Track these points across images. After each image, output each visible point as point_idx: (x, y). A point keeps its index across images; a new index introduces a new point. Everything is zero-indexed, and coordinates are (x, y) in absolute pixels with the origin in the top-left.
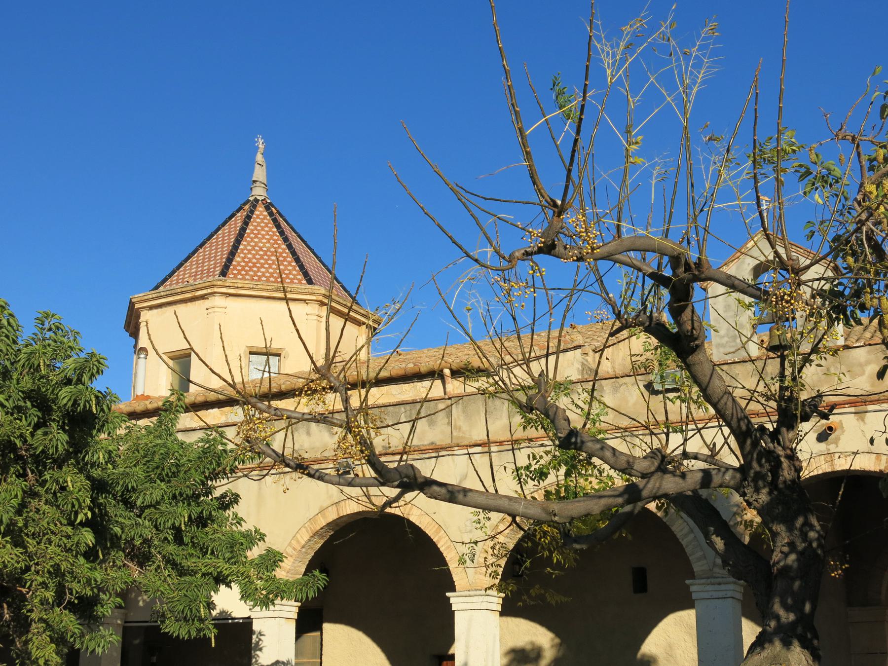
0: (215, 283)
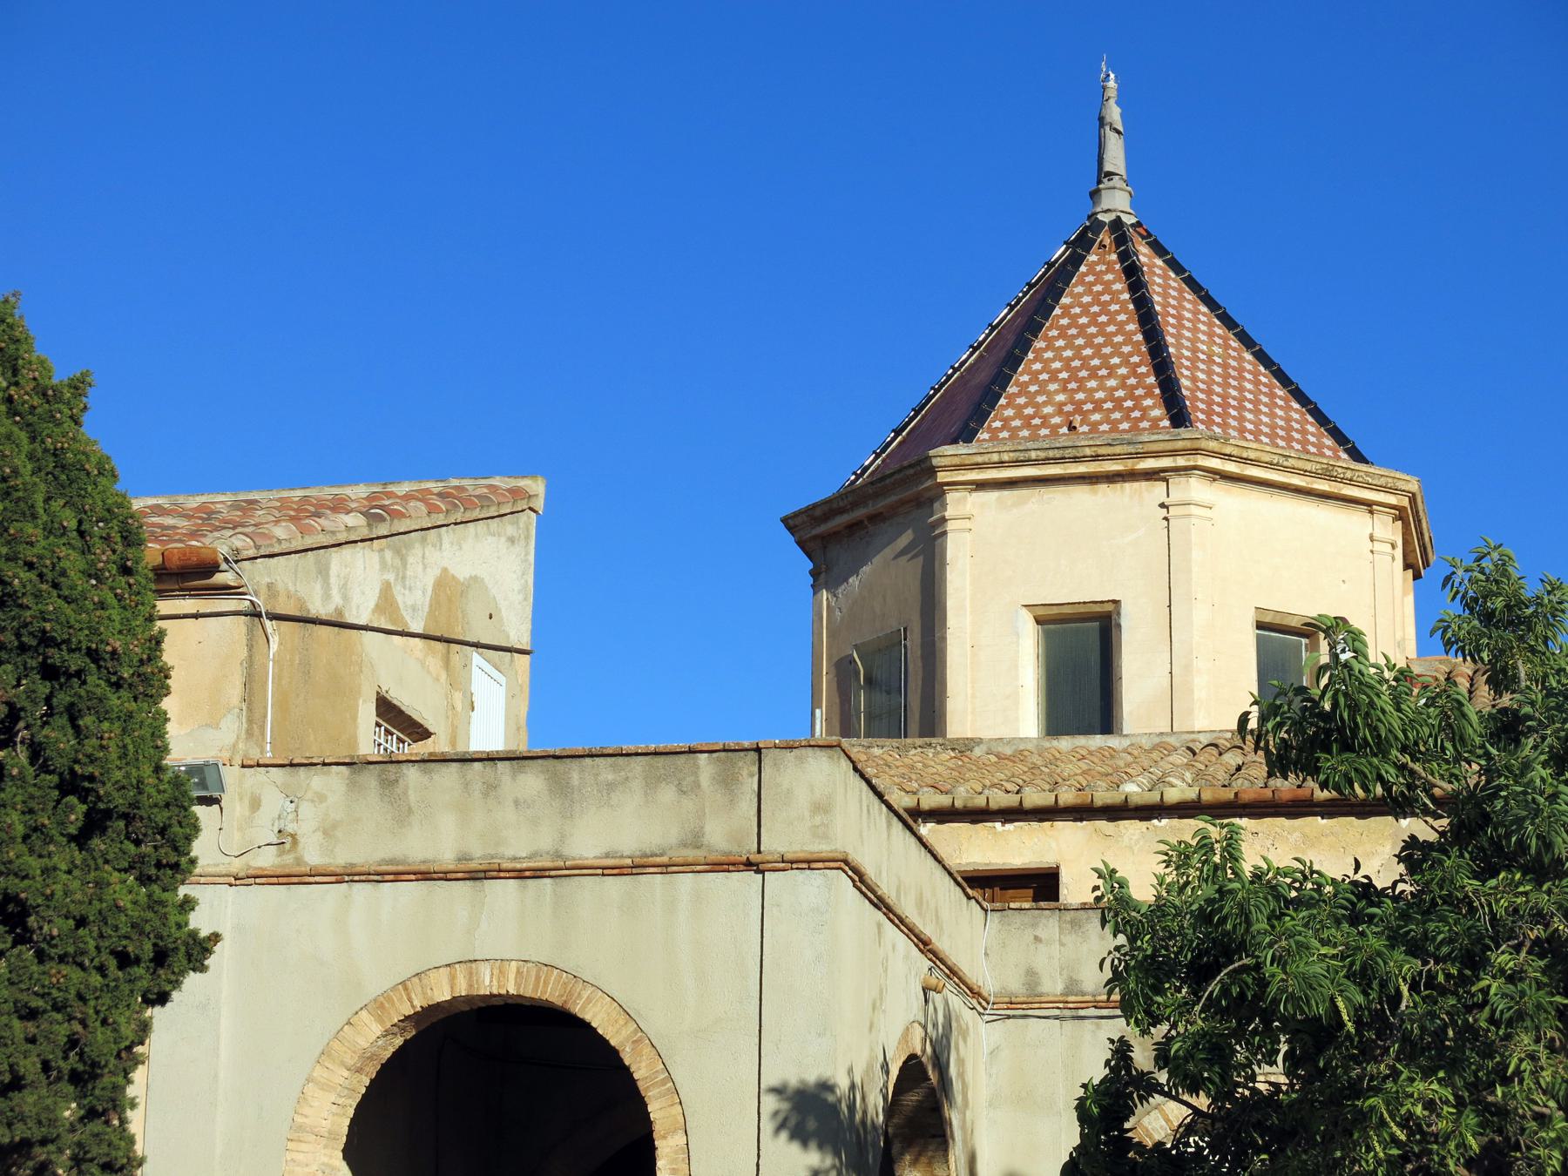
0: (1204, 444)
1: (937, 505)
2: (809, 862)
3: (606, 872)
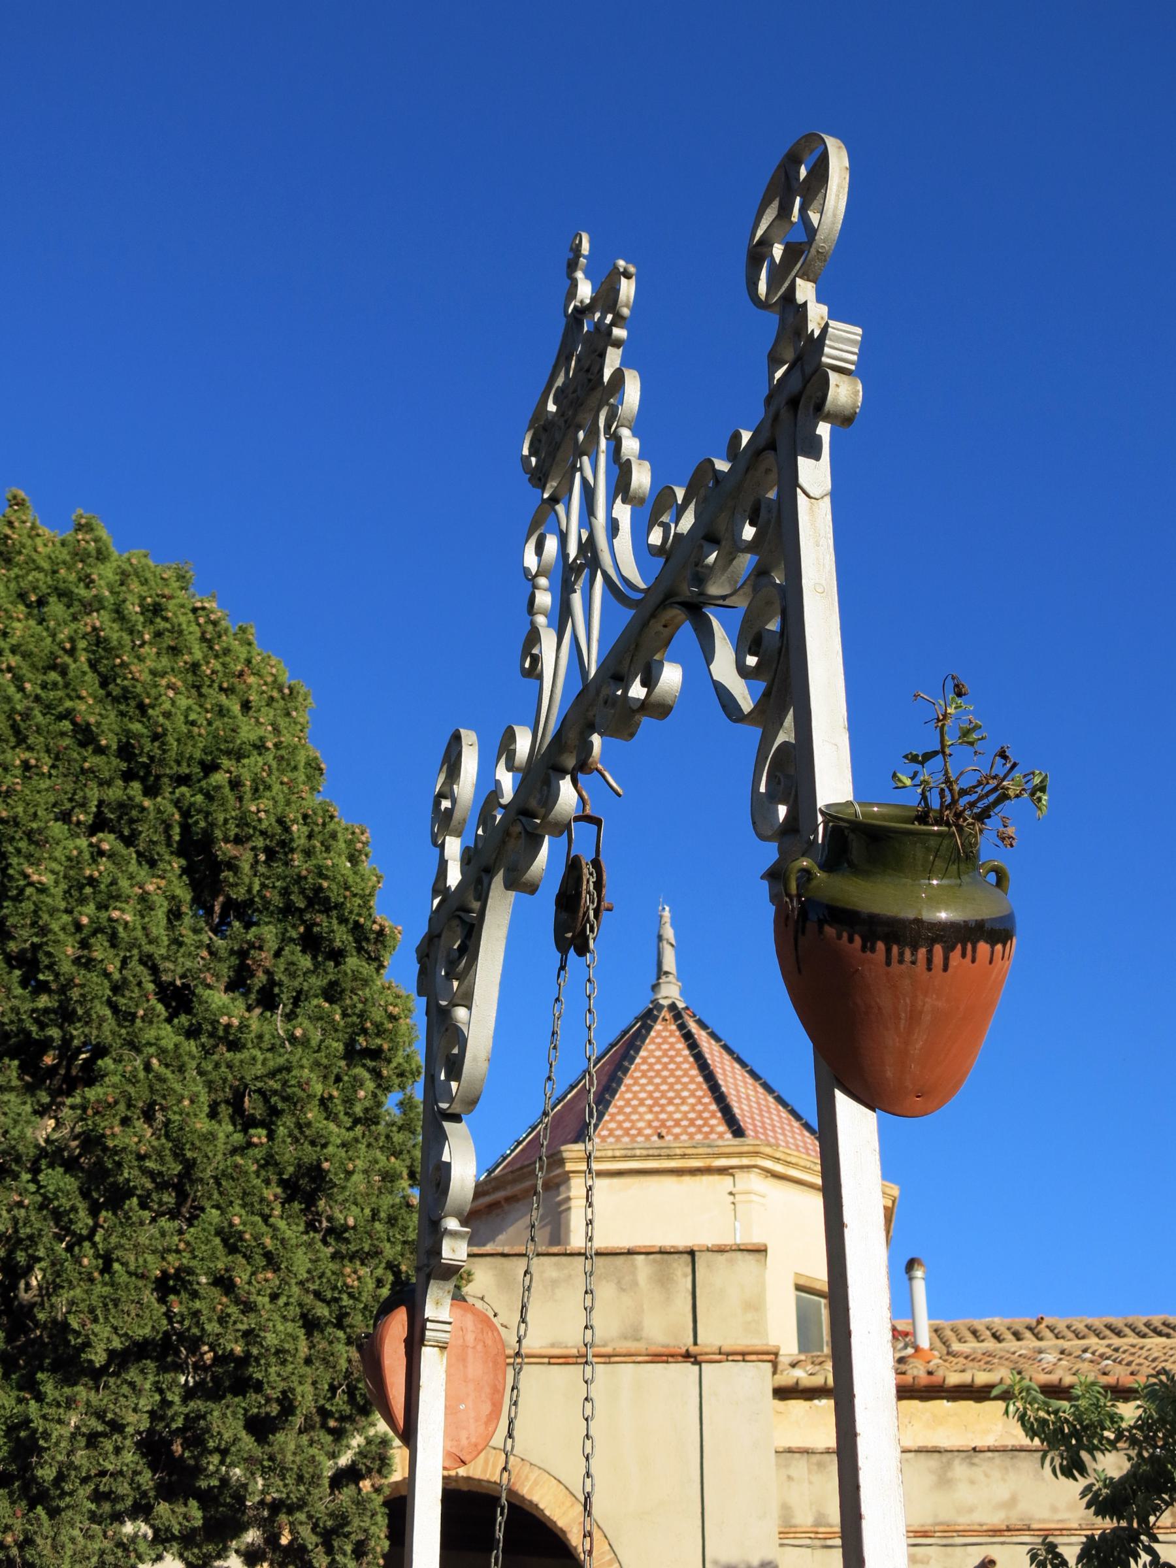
1: (562, 1188)
2: (743, 1354)
3: (552, 1361)
